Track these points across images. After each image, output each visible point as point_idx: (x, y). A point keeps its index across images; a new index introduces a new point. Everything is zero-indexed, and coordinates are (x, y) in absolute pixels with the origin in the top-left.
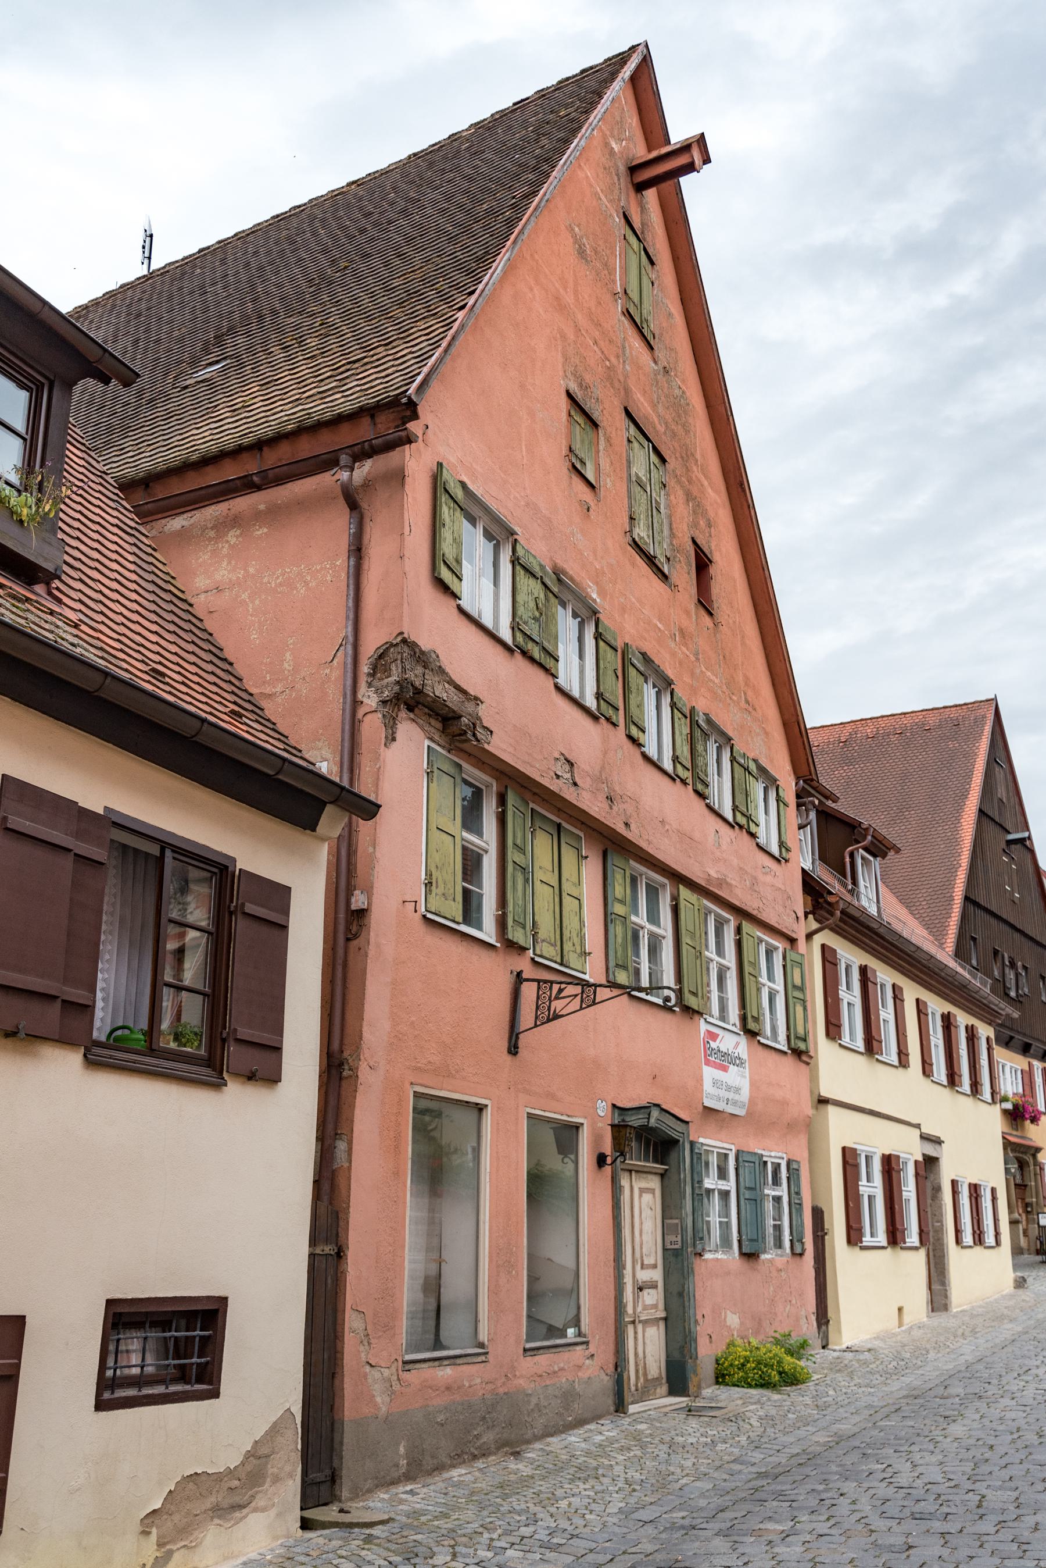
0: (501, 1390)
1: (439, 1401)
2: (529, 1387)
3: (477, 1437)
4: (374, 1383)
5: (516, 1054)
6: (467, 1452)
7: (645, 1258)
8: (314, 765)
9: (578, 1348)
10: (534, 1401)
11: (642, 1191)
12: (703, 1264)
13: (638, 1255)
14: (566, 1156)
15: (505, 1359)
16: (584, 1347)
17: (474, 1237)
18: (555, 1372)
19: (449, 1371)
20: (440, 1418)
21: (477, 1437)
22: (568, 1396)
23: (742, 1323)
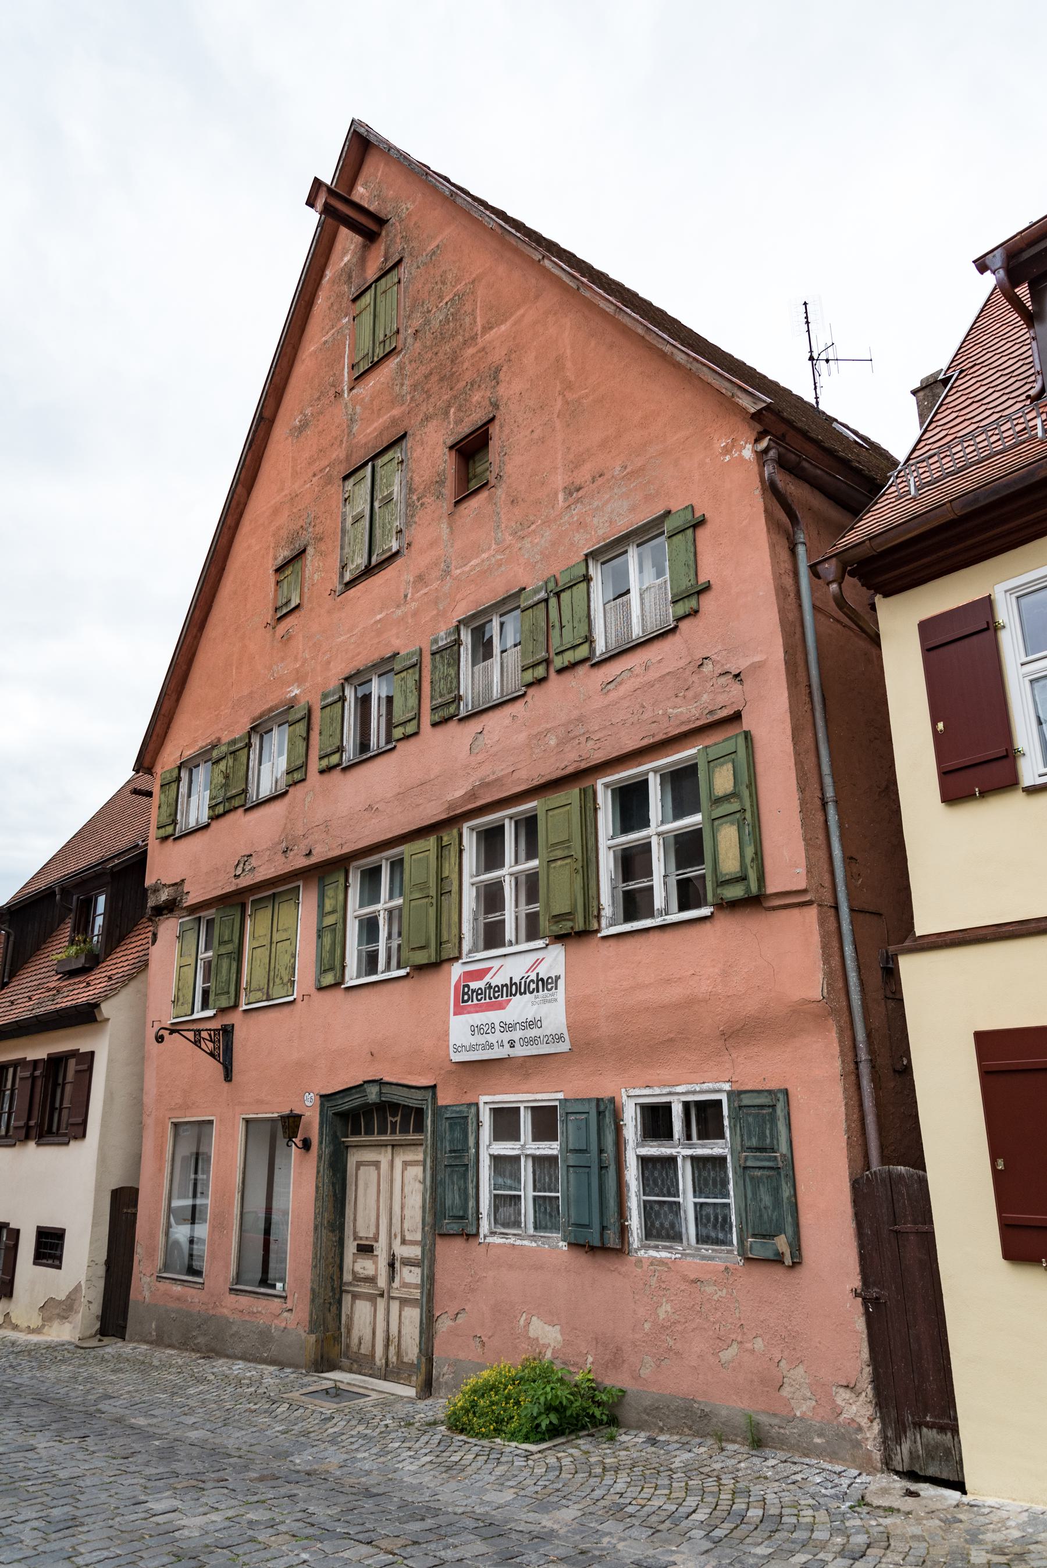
0: (211, 1312)
1: (173, 1305)
2: (235, 1317)
3: (195, 1337)
4: (145, 1284)
5: (230, 1080)
6: (185, 1344)
7: (406, 1233)
8: (638, 546)
9: (276, 1300)
10: (235, 1329)
11: (406, 1164)
12: (482, 1249)
13: (397, 1228)
14: (291, 1140)
15: (217, 1294)
16: (283, 1300)
17: (794, 1147)
18: (254, 1313)
19: (179, 1288)
20: (173, 1315)
21: (195, 1337)
22: (265, 1336)
23: (567, 1343)
